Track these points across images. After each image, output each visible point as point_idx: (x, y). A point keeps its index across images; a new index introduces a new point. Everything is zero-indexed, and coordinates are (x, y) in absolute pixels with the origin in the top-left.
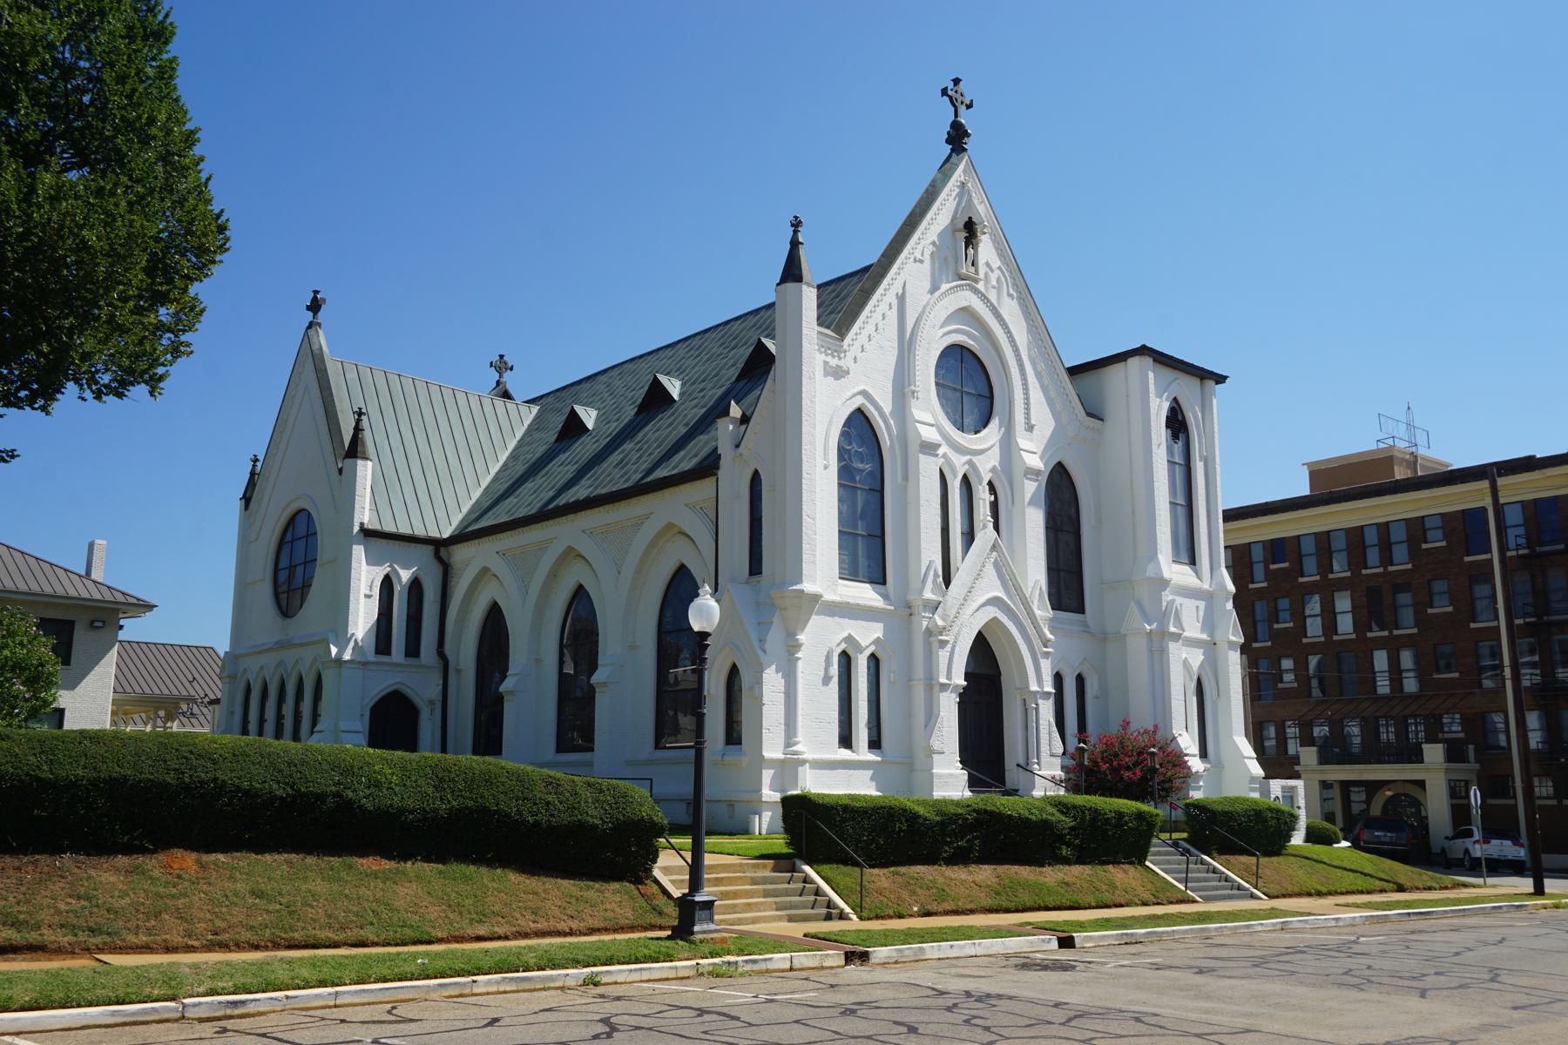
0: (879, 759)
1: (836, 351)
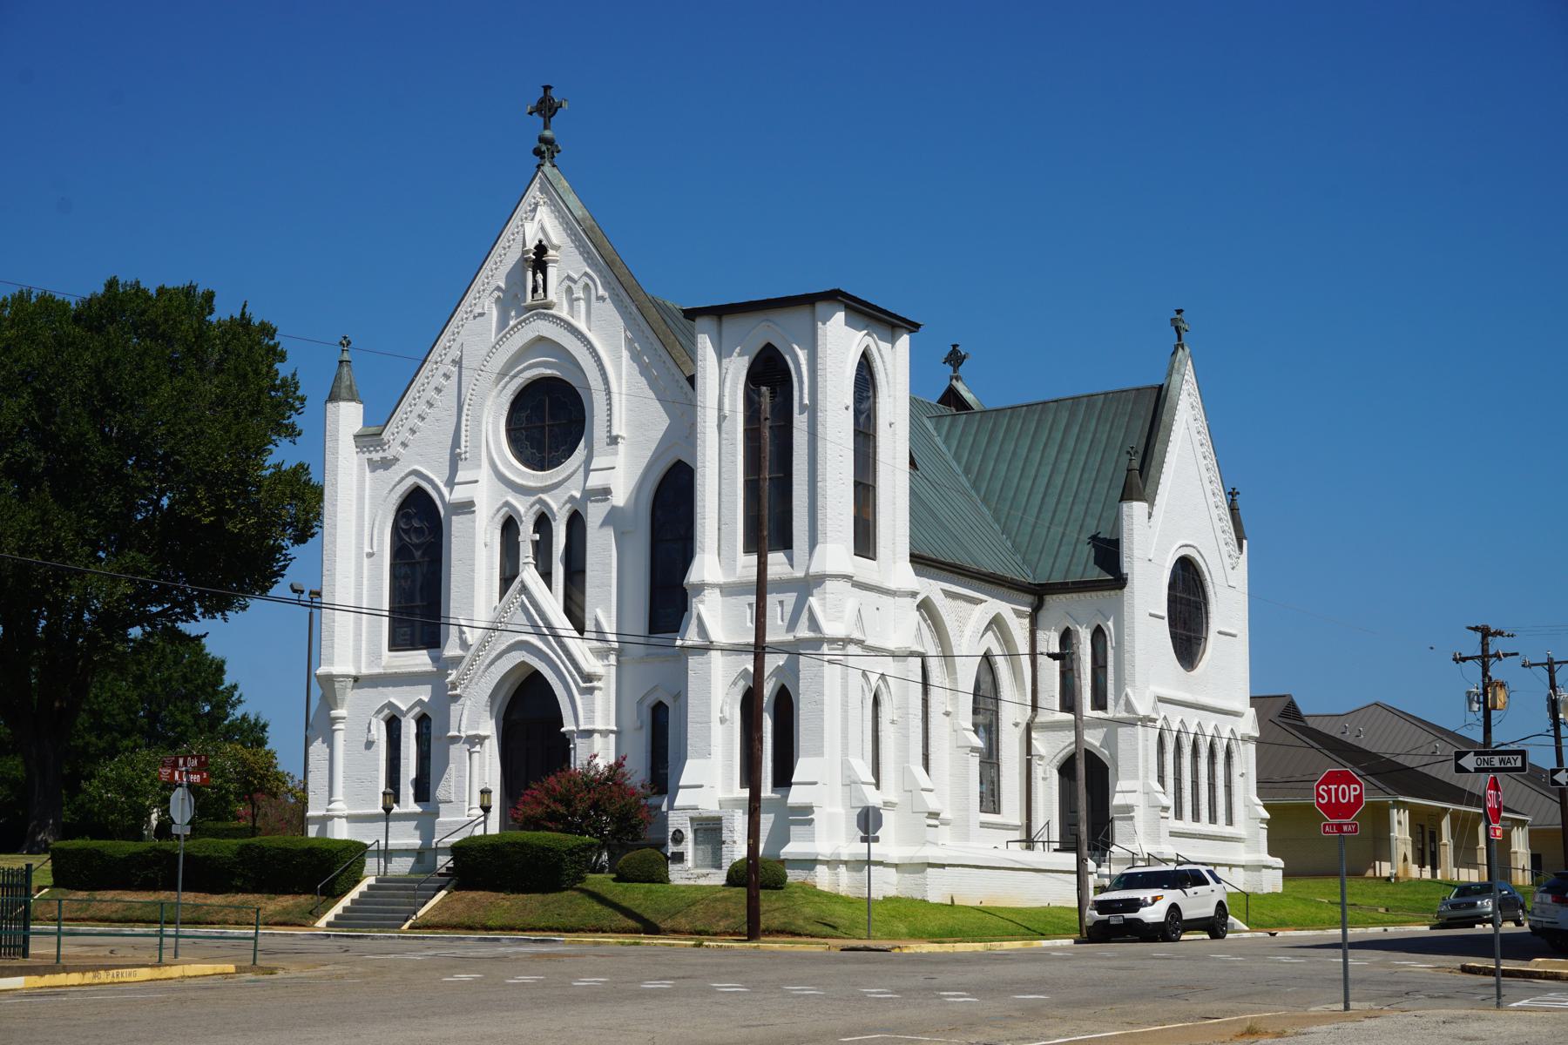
1: (378, 445)
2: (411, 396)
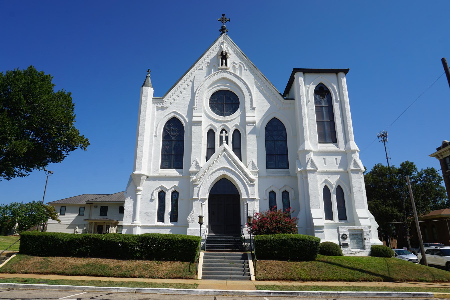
0: (173, 225)
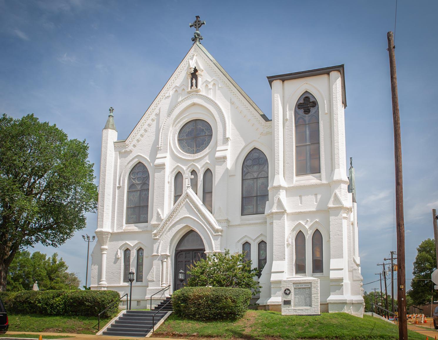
2: (138, 127)
